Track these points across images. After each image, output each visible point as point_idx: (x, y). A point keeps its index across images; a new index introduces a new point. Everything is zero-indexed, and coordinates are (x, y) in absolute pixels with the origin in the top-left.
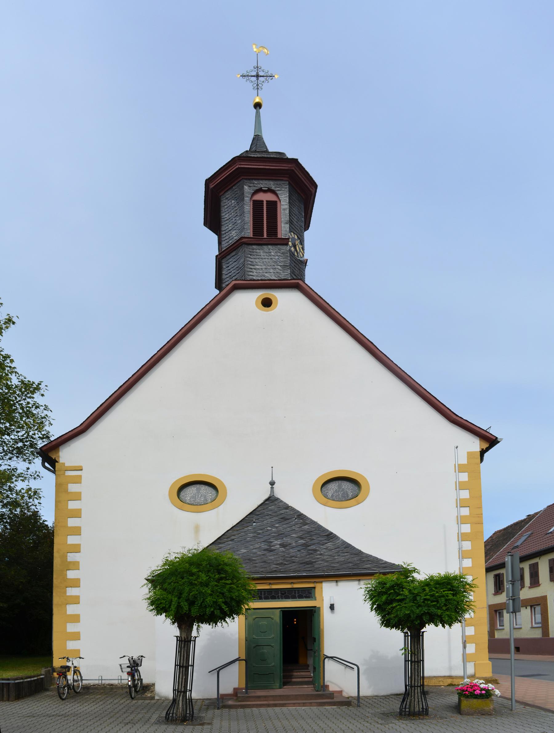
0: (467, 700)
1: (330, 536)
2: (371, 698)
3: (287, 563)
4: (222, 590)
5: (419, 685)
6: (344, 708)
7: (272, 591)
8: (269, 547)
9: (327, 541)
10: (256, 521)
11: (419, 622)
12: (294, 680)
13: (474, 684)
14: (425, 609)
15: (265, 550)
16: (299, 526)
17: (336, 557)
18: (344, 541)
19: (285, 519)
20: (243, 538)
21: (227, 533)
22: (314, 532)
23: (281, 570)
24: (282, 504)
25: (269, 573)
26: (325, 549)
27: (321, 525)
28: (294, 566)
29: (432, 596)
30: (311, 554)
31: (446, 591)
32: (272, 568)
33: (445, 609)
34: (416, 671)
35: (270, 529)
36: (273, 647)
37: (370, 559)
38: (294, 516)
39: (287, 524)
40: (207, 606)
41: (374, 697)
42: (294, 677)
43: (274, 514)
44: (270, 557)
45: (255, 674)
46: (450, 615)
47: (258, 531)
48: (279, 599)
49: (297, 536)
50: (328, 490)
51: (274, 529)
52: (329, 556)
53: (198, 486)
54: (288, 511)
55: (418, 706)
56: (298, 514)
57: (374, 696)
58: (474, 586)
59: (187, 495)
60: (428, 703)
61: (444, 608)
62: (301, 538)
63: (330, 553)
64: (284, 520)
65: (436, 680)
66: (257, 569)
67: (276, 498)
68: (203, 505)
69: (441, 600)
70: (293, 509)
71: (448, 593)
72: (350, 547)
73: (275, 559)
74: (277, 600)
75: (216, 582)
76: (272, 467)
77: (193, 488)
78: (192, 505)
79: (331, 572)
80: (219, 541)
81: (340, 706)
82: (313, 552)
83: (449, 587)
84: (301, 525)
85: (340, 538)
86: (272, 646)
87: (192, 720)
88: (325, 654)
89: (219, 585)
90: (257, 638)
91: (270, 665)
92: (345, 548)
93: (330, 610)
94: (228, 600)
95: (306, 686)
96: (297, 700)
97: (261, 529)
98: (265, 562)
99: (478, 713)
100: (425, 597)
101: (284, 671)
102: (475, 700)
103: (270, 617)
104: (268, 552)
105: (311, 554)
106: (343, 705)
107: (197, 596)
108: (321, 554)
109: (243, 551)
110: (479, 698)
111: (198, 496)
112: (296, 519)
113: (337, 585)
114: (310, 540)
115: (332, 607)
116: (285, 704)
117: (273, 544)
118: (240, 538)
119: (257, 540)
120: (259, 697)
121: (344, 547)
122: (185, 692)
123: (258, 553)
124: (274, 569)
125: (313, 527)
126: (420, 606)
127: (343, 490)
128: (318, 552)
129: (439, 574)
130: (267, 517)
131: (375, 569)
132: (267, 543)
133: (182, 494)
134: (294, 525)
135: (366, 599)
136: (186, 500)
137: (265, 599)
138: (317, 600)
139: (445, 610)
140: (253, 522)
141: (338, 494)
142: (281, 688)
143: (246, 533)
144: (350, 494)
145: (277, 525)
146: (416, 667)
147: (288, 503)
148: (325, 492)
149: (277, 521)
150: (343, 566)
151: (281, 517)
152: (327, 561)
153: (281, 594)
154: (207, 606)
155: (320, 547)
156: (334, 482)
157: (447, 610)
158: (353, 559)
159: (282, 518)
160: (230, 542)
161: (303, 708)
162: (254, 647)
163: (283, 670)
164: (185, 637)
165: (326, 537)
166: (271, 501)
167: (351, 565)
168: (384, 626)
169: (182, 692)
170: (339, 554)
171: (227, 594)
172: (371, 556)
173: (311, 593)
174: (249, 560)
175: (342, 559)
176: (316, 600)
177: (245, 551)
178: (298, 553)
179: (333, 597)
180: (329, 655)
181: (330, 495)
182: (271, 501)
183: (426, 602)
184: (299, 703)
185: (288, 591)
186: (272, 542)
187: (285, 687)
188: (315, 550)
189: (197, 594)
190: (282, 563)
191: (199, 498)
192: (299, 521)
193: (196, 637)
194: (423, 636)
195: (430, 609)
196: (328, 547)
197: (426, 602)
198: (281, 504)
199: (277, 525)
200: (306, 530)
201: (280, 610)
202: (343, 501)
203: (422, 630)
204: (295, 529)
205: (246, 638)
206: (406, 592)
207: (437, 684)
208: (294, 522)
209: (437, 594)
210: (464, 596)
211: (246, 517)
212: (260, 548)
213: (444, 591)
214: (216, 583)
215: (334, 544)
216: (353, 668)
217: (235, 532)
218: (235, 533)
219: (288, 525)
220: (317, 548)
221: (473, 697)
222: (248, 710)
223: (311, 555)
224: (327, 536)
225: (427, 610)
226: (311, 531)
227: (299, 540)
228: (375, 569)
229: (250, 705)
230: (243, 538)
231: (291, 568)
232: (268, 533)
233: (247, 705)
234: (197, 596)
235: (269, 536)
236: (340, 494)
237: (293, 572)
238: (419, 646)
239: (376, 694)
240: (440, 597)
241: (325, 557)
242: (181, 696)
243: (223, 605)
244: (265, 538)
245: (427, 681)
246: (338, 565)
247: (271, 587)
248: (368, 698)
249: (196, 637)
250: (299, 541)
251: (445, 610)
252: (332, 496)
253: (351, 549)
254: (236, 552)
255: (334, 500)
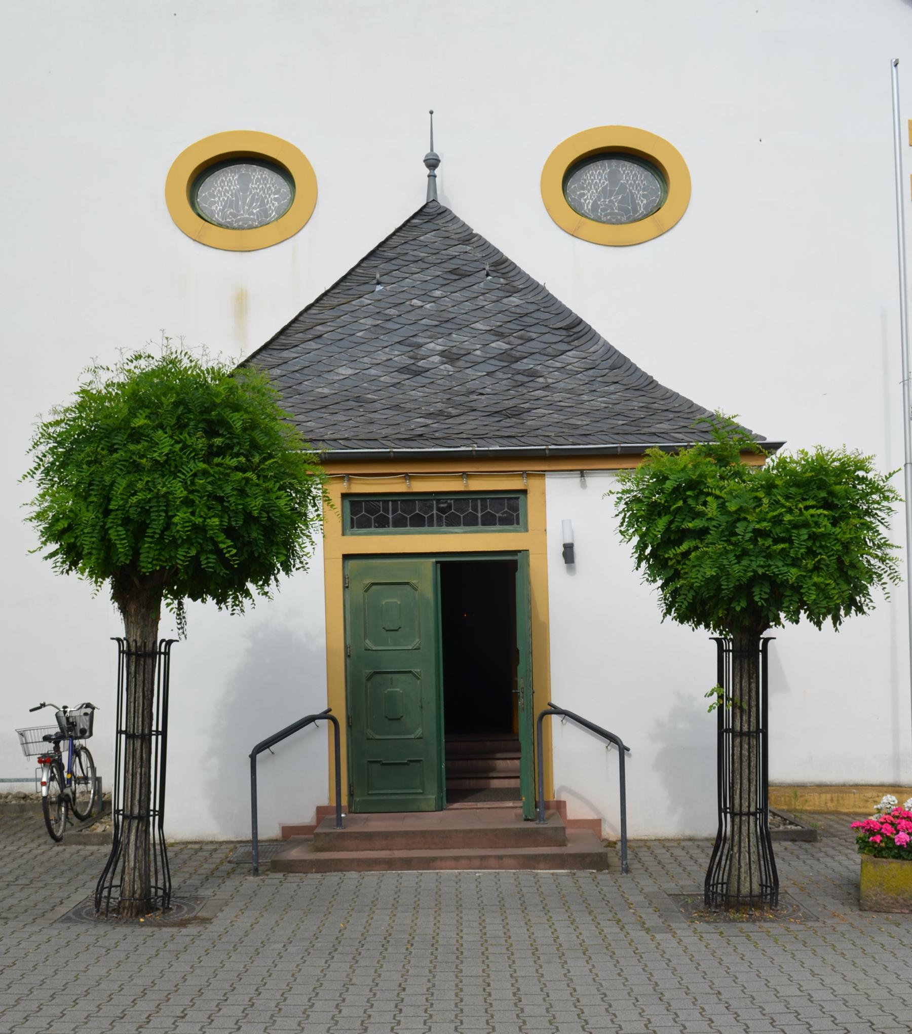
0: (875, 863)
1: (575, 330)
2: (675, 844)
3: (453, 411)
4: (221, 488)
5: (752, 809)
6: (584, 875)
7: (413, 501)
8: (412, 361)
9: (565, 347)
10: (385, 279)
11: (744, 604)
12: (496, 784)
13: (905, 812)
14: (757, 564)
15: (401, 370)
16: (494, 298)
17: (585, 397)
18: (610, 348)
19: (459, 274)
20: (347, 330)
21: (305, 315)
22: (534, 315)
23: (437, 435)
24: (455, 226)
25: (404, 443)
26: (558, 369)
27: (553, 297)
28: (471, 423)
29: (777, 521)
30: (522, 384)
31: (813, 507)
32: (413, 427)
33: (810, 566)
34: (745, 764)
35: (419, 303)
36: (418, 679)
37: (671, 405)
38: (482, 267)
39: (464, 288)
40: (179, 542)
41: (683, 844)
42: (495, 775)
43: (433, 259)
44: (413, 393)
45: (371, 762)
46: (823, 586)
47: (387, 312)
48: (431, 525)
49: (488, 328)
50: (583, 189)
51: (428, 306)
52: (570, 391)
53: (243, 169)
54: (469, 248)
55: (748, 879)
56: (496, 258)
57: (684, 840)
58: (891, 495)
59: (214, 197)
60: (778, 866)
61: (810, 564)
62: (500, 335)
63: (570, 384)
64: (457, 277)
65: (857, 796)
66: (373, 428)
67: (440, 207)
68: (256, 227)
69: (799, 535)
70: (484, 245)
71: (819, 515)
72: (625, 368)
73: (425, 399)
74: (426, 528)
75: (204, 461)
76: (431, 113)
77: (230, 177)
78: (227, 228)
79: (564, 441)
80: (283, 340)
81: (578, 869)
82: (526, 379)
83: (823, 494)
84: (502, 294)
85: (600, 337)
86: (415, 676)
87: (167, 909)
88: (554, 702)
89: (211, 471)
90: (374, 648)
91: (412, 736)
92: (612, 368)
93: (562, 560)
94: (238, 523)
95: (510, 804)
96: (469, 845)
97: (396, 305)
98: (397, 407)
99: (902, 906)
100: (757, 526)
101: (451, 755)
102: (894, 865)
103: (407, 583)
104: (408, 376)
105: (522, 384)
106: (584, 867)
107: (151, 507)
108: (547, 387)
109: (344, 372)
110: (905, 857)
111: (245, 198)
112: (488, 275)
113: (583, 485)
114: (520, 342)
115: (568, 553)
116: (434, 859)
117: (422, 351)
118: (339, 330)
119: (382, 337)
120: (369, 837)
121: (608, 366)
122: (143, 819)
123: (382, 379)
124: (419, 431)
125: (532, 300)
126: (745, 553)
127: (623, 188)
128: (541, 380)
129: (803, 452)
130: (414, 268)
131: (680, 436)
132: (409, 349)
133: (203, 192)
134: (483, 294)
135: (623, 529)
136: (213, 212)
137: (483, 524)
138: (530, 531)
139: (812, 571)
140: (375, 282)
141: (611, 201)
142: (442, 810)
143: (354, 314)
144: (642, 203)
145: (438, 293)
146: (745, 753)
147: (472, 227)
148: (574, 192)
149: (441, 281)
150: (599, 425)
151: (450, 266)
152: (561, 410)
153: (439, 509)
154: (179, 542)
155: (546, 364)
156: (599, 163)
157: (817, 568)
158: (628, 403)
159: (452, 272)
160: (312, 345)
161: (480, 872)
162: (369, 679)
163: (446, 754)
164: (136, 641)
165: (564, 332)
166: (427, 218)
167: (621, 422)
168: (675, 618)
169: (135, 818)
170: (594, 388)
171: (232, 499)
172: (676, 396)
173: (516, 509)
174: (357, 399)
175: (600, 403)
176: (527, 530)
177: (350, 372)
178: (488, 381)
179: (570, 521)
180: (563, 706)
181: (588, 205)
182: (427, 218)
183: (760, 541)
184: (469, 858)
185: (456, 500)
186: (420, 346)
187: (456, 805)
188: (533, 374)
189: (150, 500)
190: (441, 413)
191: (246, 207)
192: (496, 280)
193: (169, 643)
194: (167, 654)
195: (770, 566)
196: (569, 364)
197: (760, 541)
198: (452, 227)
199: (438, 293)
200: (513, 309)
201: (434, 560)
202: (622, 223)
203: (766, 634)
204: (483, 307)
205: (346, 647)
206: (712, 508)
207: (859, 807)
208: (482, 284)
209: (788, 517)
210: (869, 527)
211: (358, 265)
212: (388, 363)
213: (807, 508)
214: (202, 466)
215: (584, 355)
216: (421, 760)
217: (327, 312)
218: (328, 314)
219: (467, 293)
220: (539, 368)
221: (893, 853)
222: (332, 878)
223: (520, 389)
224: (567, 328)
225: (762, 567)
226: (526, 315)
227: (493, 342)
228: (680, 436)
229: (340, 861)
230: (347, 330)
231: (463, 427)
232: (412, 317)
233: (332, 860)
234: (151, 507)
235: (415, 328)
236: (616, 199)
237: (469, 442)
238: (753, 685)
239: (689, 833)
240: (796, 526)
241: (557, 397)
242: (134, 831)
243: (222, 537)
244: (406, 332)
245: (835, 799)
246: (586, 421)
247: (467, 486)
248: (667, 844)
249: (169, 643)
250: (493, 345)
251: (812, 571)
252: (595, 206)
253: (628, 373)
254: (325, 375)
255: (598, 220)
